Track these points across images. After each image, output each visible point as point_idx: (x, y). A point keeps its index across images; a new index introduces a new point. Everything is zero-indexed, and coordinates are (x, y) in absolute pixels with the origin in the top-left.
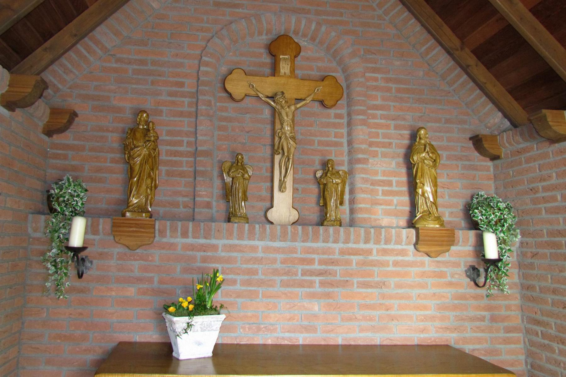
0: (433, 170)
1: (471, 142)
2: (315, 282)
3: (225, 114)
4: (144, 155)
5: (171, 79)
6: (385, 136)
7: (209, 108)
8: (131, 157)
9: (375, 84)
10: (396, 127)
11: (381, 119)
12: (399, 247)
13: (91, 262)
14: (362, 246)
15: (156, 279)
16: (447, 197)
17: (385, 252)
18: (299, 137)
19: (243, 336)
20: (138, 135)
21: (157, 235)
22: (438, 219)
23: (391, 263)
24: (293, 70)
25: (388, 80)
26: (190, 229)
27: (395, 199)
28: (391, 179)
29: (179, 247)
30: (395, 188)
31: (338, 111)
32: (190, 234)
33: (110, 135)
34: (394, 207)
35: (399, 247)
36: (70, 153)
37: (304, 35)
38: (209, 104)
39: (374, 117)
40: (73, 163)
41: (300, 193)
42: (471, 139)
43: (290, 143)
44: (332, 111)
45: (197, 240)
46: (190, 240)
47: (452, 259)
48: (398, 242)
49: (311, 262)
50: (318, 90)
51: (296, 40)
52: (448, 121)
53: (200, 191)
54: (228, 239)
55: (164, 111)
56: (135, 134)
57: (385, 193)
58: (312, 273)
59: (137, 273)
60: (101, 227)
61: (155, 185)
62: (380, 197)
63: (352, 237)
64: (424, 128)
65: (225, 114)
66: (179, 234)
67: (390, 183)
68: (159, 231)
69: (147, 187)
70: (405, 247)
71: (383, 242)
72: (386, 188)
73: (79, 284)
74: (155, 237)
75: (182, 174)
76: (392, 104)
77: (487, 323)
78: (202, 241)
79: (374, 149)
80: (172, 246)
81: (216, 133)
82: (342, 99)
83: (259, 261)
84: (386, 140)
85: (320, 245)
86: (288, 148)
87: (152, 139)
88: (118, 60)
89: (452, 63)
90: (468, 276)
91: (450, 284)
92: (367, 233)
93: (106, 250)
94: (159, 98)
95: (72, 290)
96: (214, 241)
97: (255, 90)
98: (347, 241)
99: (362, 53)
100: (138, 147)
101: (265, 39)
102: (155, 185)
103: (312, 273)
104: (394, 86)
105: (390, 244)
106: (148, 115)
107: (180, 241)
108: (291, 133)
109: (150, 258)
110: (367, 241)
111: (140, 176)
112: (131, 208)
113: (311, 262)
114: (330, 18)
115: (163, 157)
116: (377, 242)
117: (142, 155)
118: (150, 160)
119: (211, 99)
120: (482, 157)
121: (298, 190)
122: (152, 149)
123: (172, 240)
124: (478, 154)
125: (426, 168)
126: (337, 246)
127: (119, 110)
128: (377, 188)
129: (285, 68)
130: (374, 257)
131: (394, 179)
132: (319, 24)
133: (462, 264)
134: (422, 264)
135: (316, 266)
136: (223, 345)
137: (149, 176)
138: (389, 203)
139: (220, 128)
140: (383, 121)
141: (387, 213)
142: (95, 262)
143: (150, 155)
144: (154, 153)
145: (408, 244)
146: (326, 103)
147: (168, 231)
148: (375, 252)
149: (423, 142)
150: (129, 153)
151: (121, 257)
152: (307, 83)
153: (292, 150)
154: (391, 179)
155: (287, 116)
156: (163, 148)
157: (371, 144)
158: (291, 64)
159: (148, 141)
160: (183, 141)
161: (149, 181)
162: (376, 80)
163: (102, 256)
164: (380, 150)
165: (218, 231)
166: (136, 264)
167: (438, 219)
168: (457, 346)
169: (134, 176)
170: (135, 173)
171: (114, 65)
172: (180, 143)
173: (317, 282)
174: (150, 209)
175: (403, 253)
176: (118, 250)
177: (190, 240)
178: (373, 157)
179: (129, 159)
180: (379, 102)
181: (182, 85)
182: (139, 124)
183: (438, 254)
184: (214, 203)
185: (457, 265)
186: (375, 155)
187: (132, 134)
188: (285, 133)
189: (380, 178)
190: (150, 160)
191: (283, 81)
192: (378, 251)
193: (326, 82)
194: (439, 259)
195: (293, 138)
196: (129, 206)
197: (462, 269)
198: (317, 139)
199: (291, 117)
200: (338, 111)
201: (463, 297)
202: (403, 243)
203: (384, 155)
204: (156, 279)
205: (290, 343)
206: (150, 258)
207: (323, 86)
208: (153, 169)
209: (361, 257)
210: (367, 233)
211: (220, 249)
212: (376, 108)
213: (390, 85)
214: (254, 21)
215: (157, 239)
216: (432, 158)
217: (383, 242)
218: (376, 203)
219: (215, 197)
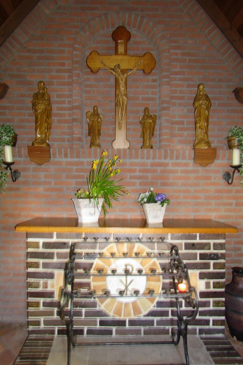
0: (207, 112)
1: (234, 93)
2: (137, 183)
3: (88, 83)
4: (43, 109)
5: (58, 61)
6: (181, 92)
7: (78, 78)
8: (36, 111)
9: (176, 57)
10: (188, 86)
11: (179, 81)
12: (184, 161)
13: (20, 173)
14: (163, 161)
15: (53, 183)
16: (216, 131)
17: (176, 165)
18: (130, 95)
19: (173, 216)
20: (39, 97)
21: (52, 156)
22: (208, 143)
23: (179, 171)
24: (126, 50)
25: (184, 54)
26: (69, 152)
27: (185, 133)
28: (183, 120)
29: (64, 164)
30: (185, 126)
31: (154, 77)
32: (69, 156)
33: (26, 99)
34: (184, 138)
35: (184, 161)
36: (7, 111)
37: (134, 26)
38: (78, 76)
39: (175, 79)
40: (9, 117)
41: (131, 131)
42: (233, 92)
43: (123, 98)
44: (150, 78)
45: (73, 159)
46: (69, 160)
47: (216, 168)
48: (184, 158)
49: (134, 171)
50: (140, 62)
51: (128, 30)
52: (220, 81)
53: (75, 131)
54: (89, 158)
55: (55, 82)
56: (37, 96)
57: (180, 129)
58: (135, 177)
59: (43, 179)
60: (23, 152)
61: (50, 127)
62: (176, 132)
63: (157, 155)
64: (203, 84)
65: (88, 83)
66: (63, 155)
67: (182, 123)
68: (53, 154)
69: (45, 128)
70: (188, 161)
71: (175, 158)
72: (181, 126)
73: (14, 185)
74: (50, 157)
75: (65, 122)
76: (186, 70)
77: (233, 206)
78: (76, 160)
79: (174, 101)
80: (60, 163)
81: (84, 95)
82: (155, 68)
83: (139, 178)
84: (182, 95)
85: (139, 160)
86: (123, 101)
87: (47, 98)
88: (29, 51)
89: (225, 39)
90: (225, 179)
91: (213, 184)
92: (166, 152)
93: (27, 166)
94: (52, 74)
95: (10, 189)
96: (82, 160)
97: (104, 64)
98: (154, 158)
99: (169, 36)
100: (39, 104)
101: (111, 30)
102: (50, 127)
103: (135, 177)
104: (187, 58)
105: (179, 159)
106: (44, 84)
107: (64, 160)
108: (124, 91)
109: (49, 170)
110: (166, 158)
111: (41, 122)
112: (37, 140)
113: (134, 171)
114: (150, 13)
115: (54, 111)
116: (171, 158)
117: (42, 109)
118: (46, 112)
119: (79, 72)
120: (239, 104)
121: (130, 129)
122: (47, 105)
123: (60, 160)
124: (237, 102)
125: (202, 110)
126: (150, 161)
127: (30, 83)
128: (175, 126)
129: (121, 49)
130: (170, 168)
131: (185, 120)
132: (143, 17)
133: (221, 171)
134: (197, 172)
135: (137, 174)
136: (169, 220)
137: (46, 121)
138: (181, 136)
139: (87, 92)
140: (179, 82)
141: (181, 142)
142: (22, 173)
143: (46, 109)
144: (48, 107)
145: (189, 159)
146: (146, 71)
147: (57, 154)
148: (170, 164)
149: (201, 93)
150: (35, 108)
151: (34, 170)
152: (134, 58)
153: (125, 103)
154: (183, 120)
155: (122, 80)
156: (54, 106)
157: (172, 98)
158: (125, 46)
159: (44, 99)
160: (65, 101)
161: (46, 124)
162: (177, 54)
163: (25, 170)
164: (177, 101)
165: (83, 153)
166: (42, 174)
167: (208, 143)
168: (216, 220)
169: (38, 121)
170: (39, 119)
171: (27, 54)
172: (64, 102)
173: (138, 183)
174: (48, 142)
175: (186, 165)
176: (33, 166)
177: (69, 160)
178: (174, 106)
179: (35, 112)
180: (178, 70)
181: (63, 64)
182: (40, 90)
183: (206, 165)
184: (84, 139)
185: (218, 172)
186: (174, 105)
187: (36, 96)
188: (121, 92)
189: (177, 119)
190: (46, 112)
191: (120, 57)
192: (172, 164)
193: (146, 57)
194: (207, 168)
195: (126, 95)
196: (37, 140)
197: (221, 175)
198: (141, 96)
199: (124, 81)
200: (154, 77)
201: (220, 191)
202: (187, 158)
203: (180, 105)
204: (53, 183)
205: (123, 218)
206: (49, 170)
207: (144, 60)
208: (48, 117)
209: (163, 168)
210: (166, 152)
211: (85, 164)
212: (177, 73)
213: (185, 57)
214: (104, 18)
215: (52, 159)
216: (206, 104)
217: (175, 158)
218: (173, 136)
219: (84, 135)
